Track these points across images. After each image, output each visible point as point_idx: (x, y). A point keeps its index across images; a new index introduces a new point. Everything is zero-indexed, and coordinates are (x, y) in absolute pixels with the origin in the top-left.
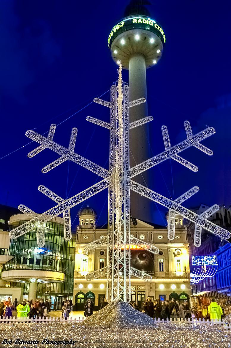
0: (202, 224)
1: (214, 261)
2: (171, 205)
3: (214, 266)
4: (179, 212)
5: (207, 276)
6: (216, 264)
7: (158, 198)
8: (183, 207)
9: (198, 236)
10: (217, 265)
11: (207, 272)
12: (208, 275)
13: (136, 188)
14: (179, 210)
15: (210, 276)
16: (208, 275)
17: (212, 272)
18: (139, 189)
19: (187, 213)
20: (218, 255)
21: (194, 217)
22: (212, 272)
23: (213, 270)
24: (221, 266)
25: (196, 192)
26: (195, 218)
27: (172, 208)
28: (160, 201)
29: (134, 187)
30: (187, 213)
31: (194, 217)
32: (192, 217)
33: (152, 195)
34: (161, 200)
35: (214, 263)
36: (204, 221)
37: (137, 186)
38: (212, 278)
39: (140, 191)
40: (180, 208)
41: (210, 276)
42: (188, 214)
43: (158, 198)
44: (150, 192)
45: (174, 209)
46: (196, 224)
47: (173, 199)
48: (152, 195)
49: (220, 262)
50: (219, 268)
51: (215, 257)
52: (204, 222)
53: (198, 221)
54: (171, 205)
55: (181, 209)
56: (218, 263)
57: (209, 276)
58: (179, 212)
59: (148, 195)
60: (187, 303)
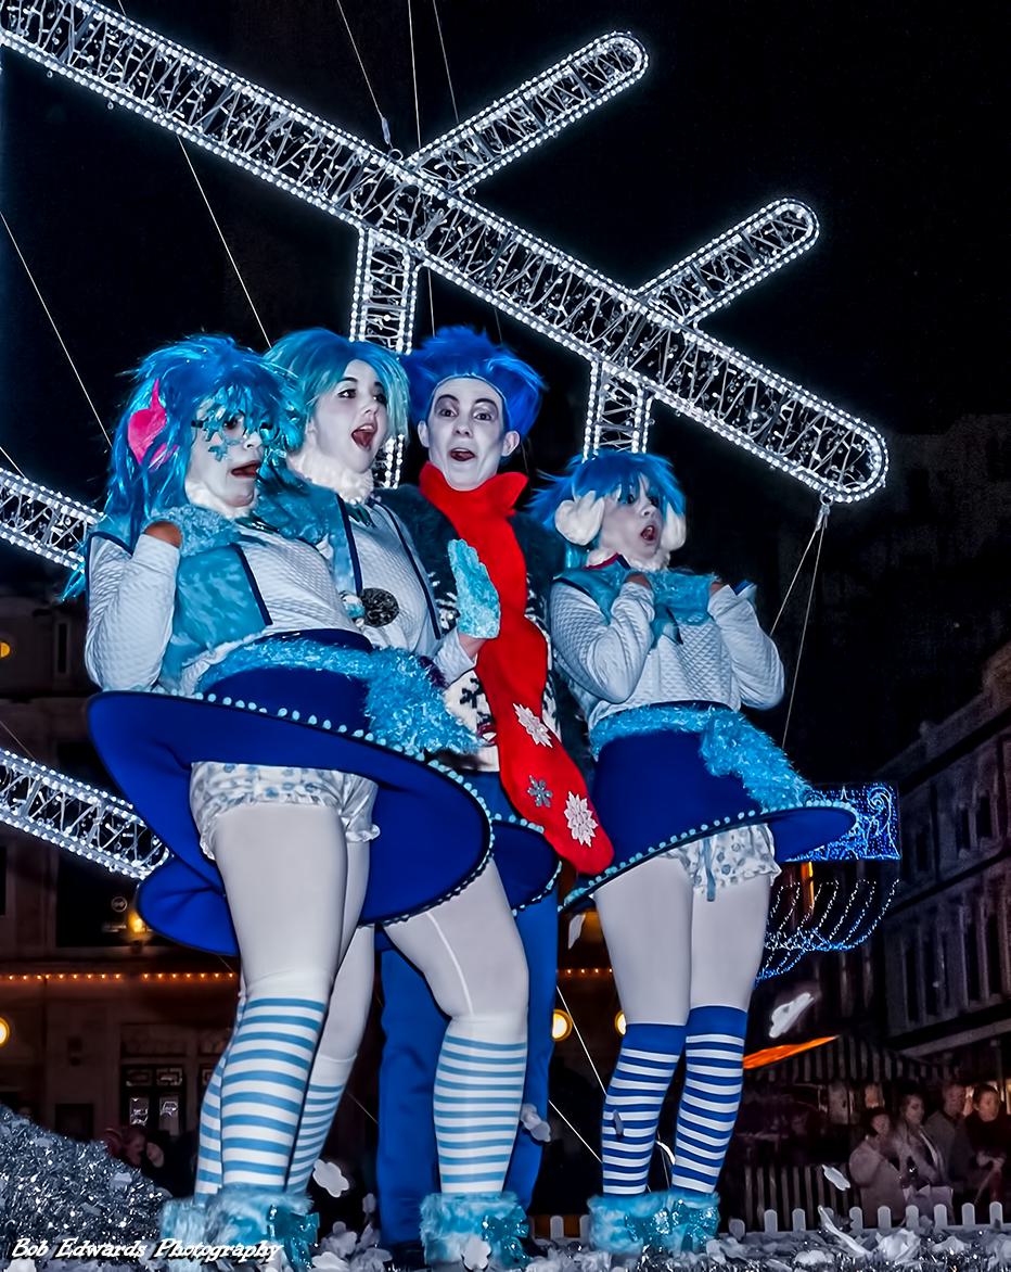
0: (656, 368)
1: (874, 830)
2: (379, 197)
3: (874, 868)
4: (455, 255)
5: (816, 941)
6: (889, 849)
7: (261, 134)
8: (490, 221)
9: (290, 151)
10: (896, 856)
11: (821, 906)
12: (825, 932)
13: (63, 37)
14: (448, 246)
15: (841, 946)
16: (825, 932)
17: (838, 910)
18: (92, 50)
19: (525, 272)
20: (903, 787)
21: (590, 309)
22: (838, 910)
23: (866, 889)
24: (924, 866)
25: (618, 82)
26: (598, 312)
27: (387, 225)
28: (283, 159)
29: (48, 24)
30: (525, 272)
31: (590, 309)
32: (569, 309)
33: (209, 102)
34: (292, 148)
35: (875, 845)
36: (677, 339)
37: (71, 20)
38: (855, 957)
39: (96, 63)
40: (465, 220)
41: (841, 946)
42: (540, 281)
43: (261, 134)
44: (189, 76)
45: (403, 234)
46: (607, 370)
47: (405, 143)
48: (209, 102)
49: (922, 839)
50: (906, 875)
51: (881, 797)
52: (678, 356)
53: (617, 338)
54: (379, 197)
55: (475, 236)
56: (904, 846)
57: (835, 941)
58: (455, 255)
59: (177, 99)
60: (598, 1237)
